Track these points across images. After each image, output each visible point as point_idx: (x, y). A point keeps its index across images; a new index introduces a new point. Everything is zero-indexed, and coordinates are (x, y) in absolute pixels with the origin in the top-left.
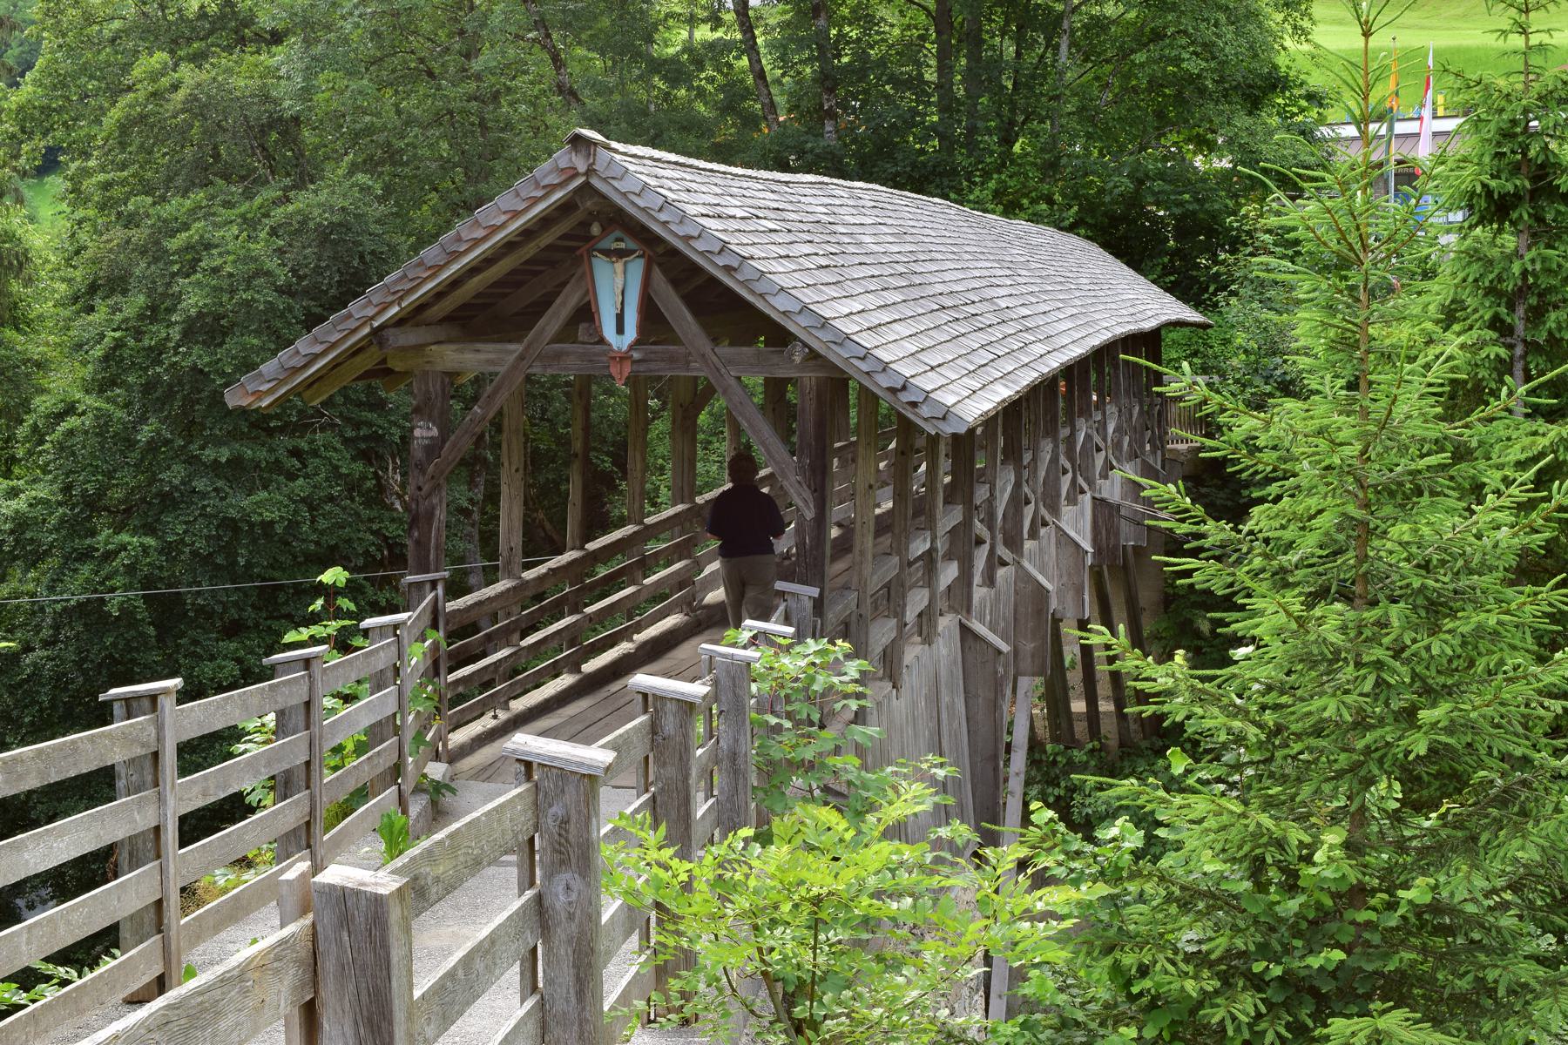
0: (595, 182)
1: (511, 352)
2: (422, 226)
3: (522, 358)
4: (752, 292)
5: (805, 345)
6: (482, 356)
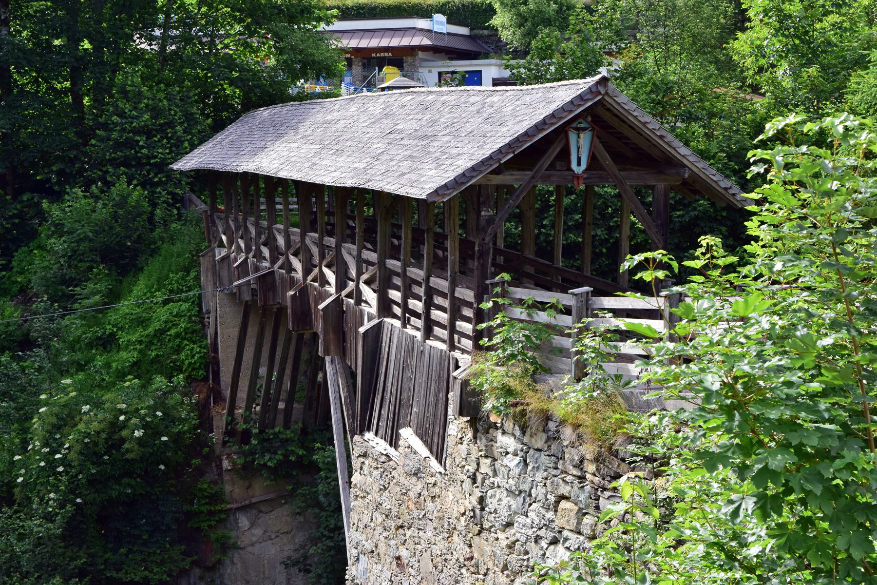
0: (606, 98)
1: (526, 175)
2: (68, 193)
3: (533, 177)
4: (670, 146)
5: (690, 169)
6: (513, 177)
